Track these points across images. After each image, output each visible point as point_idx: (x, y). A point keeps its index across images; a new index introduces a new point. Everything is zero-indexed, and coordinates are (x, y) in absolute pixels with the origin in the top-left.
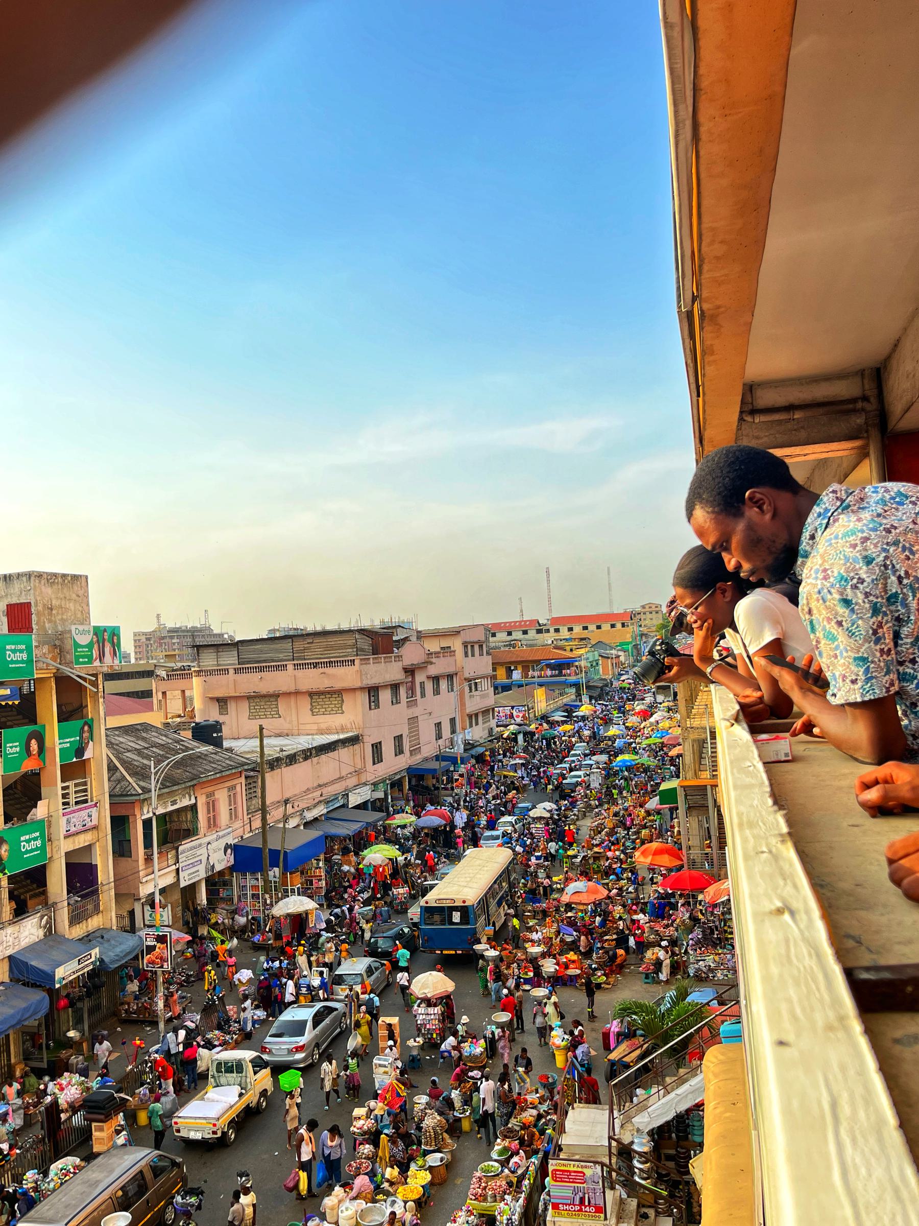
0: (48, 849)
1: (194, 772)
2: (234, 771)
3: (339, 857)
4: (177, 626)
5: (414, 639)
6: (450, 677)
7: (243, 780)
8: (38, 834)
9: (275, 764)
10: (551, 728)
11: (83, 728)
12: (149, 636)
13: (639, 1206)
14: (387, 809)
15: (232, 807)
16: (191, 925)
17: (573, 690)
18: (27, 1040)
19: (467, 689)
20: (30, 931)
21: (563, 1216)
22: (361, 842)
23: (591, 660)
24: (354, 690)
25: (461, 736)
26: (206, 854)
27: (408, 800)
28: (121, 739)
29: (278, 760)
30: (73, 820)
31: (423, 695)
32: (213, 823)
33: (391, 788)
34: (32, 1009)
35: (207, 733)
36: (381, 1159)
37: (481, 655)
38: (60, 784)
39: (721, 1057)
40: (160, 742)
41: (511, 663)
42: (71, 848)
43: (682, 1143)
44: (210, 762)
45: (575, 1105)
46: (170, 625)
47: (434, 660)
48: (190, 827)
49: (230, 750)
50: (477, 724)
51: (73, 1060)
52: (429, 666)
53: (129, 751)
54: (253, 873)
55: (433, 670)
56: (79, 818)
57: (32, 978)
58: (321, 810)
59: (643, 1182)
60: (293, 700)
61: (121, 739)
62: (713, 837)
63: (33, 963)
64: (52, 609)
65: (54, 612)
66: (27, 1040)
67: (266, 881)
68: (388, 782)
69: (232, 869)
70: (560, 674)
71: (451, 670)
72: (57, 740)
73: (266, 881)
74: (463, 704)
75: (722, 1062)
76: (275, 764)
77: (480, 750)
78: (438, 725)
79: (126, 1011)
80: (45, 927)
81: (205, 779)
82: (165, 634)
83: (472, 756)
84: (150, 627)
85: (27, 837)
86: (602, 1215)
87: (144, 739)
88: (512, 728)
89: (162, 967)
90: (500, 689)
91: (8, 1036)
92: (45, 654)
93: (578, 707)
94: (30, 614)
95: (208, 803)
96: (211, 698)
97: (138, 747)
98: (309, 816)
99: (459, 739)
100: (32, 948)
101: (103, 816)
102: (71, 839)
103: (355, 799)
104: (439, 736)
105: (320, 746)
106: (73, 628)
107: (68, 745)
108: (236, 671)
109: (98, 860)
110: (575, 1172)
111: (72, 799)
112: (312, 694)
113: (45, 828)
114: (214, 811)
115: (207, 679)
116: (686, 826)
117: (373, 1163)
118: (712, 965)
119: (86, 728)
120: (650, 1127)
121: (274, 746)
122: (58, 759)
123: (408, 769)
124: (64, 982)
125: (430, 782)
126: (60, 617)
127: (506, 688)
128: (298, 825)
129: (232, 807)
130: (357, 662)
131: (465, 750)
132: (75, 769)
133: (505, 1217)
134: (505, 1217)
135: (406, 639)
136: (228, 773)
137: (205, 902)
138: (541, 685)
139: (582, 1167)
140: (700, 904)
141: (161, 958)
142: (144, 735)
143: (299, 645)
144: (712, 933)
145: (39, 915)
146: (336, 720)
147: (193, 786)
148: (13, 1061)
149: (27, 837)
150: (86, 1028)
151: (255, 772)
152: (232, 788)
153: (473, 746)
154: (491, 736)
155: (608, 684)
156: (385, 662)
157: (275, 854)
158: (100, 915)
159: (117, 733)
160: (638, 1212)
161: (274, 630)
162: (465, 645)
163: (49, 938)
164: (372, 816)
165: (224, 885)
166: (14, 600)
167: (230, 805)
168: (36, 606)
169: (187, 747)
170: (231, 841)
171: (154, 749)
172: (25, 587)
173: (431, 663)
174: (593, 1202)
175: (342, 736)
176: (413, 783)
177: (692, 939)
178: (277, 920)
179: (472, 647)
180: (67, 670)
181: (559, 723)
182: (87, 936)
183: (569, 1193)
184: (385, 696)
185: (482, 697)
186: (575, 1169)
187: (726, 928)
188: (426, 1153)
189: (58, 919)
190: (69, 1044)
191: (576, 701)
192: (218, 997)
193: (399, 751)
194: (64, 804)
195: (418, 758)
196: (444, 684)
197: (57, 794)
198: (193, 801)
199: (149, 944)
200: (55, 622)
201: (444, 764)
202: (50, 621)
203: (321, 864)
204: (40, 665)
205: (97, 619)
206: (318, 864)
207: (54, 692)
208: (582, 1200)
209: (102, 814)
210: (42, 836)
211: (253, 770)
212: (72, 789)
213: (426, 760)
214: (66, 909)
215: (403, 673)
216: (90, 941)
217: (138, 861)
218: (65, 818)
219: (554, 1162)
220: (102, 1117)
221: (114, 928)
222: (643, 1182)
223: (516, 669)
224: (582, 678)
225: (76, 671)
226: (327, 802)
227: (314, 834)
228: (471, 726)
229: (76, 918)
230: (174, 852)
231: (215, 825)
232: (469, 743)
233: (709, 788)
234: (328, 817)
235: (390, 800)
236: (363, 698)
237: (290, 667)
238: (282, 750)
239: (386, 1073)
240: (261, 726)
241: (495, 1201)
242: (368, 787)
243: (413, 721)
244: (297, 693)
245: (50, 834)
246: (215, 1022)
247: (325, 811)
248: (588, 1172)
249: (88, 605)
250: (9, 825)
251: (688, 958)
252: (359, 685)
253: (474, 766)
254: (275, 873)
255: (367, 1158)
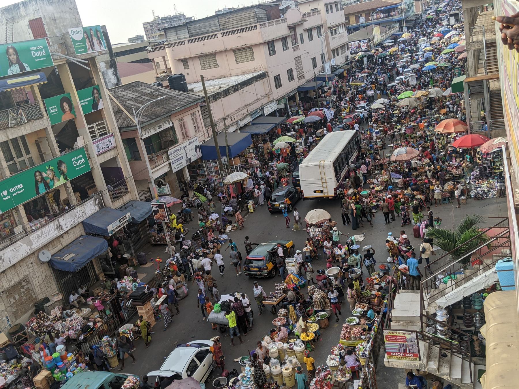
0: (90, 163)
1: (169, 108)
2: (192, 104)
3: (262, 145)
4: (166, 16)
5: (293, 6)
6: (318, 28)
7: (199, 108)
8: (81, 156)
9: (216, 97)
10: (384, 50)
11: (93, 91)
12: (151, 24)
13: (440, 350)
14: (288, 113)
15: (196, 125)
16: (185, 190)
17: (397, 25)
18: (103, 262)
19: (330, 34)
20: (90, 208)
21: (393, 358)
22: (272, 135)
23: (408, 3)
24: (259, 45)
25: (329, 64)
26: (184, 153)
27: (300, 107)
28: (124, 93)
29: (218, 94)
30: (100, 146)
31: (302, 42)
32: (186, 135)
33: (289, 101)
34: (99, 249)
35: (177, 83)
36: (291, 316)
37: (337, 10)
38: (87, 127)
39: (498, 303)
40: (147, 92)
41: (358, 12)
42: (103, 160)
43: (467, 310)
44: (177, 101)
45: (400, 291)
46: (162, 16)
47: (307, 19)
48: (173, 139)
49: (192, 90)
50: (338, 55)
51: (128, 270)
52: (304, 23)
53: (129, 100)
54: (213, 160)
55: (307, 25)
56: (104, 143)
57: (97, 232)
58: (249, 119)
59: (443, 337)
60: (224, 55)
61: (124, 93)
62: (487, 110)
63: (95, 225)
64: (55, 20)
65: (57, 21)
66: (103, 262)
67: (221, 164)
68: (286, 98)
69: (201, 159)
70: (388, 16)
71: (319, 23)
72: (79, 103)
73: (221, 164)
74: (328, 44)
75: (499, 307)
76: (216, 97)
77: (341, 71)
78: (314, 59)
79: (154, 240)
80: (98, 204)
81: (175, 112)
82: (160, 22)
83: (336, 75)
84: (151, 19)
85: (76, 158)
86: (418, 358)
87: (137, 91)
88: (360, 54)
89: (164, 220)
90: (350, 31)
91: (91, 262)
92: (56, 50)
93: (401, 35)
94: (43, 25)
95: (181, 125)
96: (178, 60)
97: (134, 97)
98: (242, 124)
99: (327, 66)
100: (93, 216)
101: (117, 140)
102: (102, 156)
103: (268, 111)
104: (315, 66)
105: (242, 82)
106: (70, 30)
107: (87, 103)
108: (189, 41)
109: (121, 165)
110: (400, 336)
111: (97, 133)
112: (235, 51)
113: (85, 151)
114: (185, 128)
115: (174, 48)
116: (471, 106)
117: (287, 318)
118: (485, 190)
119: (95, 91)
120: (447, 305)
121: (212, 87)
122: (82, 112)
123: (298, 88)
124: (114, 233)
125: (313, 95)
126: (62, 24)
127: (356, 29)
128: (236, 130)
129: (184, 131)
130: (258, 27)
131: (332, 72)
132: (94, 116)
133: (361, 352)
134: (361, 352)
135: (288, 7)
136: (188, 106)
137: (189, 178)
138: (377, 24)
139: (404, 334)
140: (478, 154)
141: (163, 216)
142: (137, 89)
143: (223, 20)
144: (486, 170)
145: (93, 199)
146: (249, 65)
147: (170, 116)
148: (97, 272)
149: (76, 158)
150: (133, 252)
151: (205, 103)
152: (193, 114)
153: (336, 69)
154: (348, 61)
155: (420, 17)
156: (276, 24)
157: (223, 148)
158: (129, 194)
159: (121, 89)
160: (440, 352)
161: (219, 11)
162: (326, 5)
163: (102, 210)
164: (278, 119)
165: (199, 168)
166: (32, 17)
167: (194, 124)
168: (45, 19)
169: (163, 93)
170: (198, 144)
171: (144, 97)
172: (35, 8)
173: (305, 21)
174: (412, 351)
175: (255, 74)
176: (302, 96)
177: (473, 175)
178: (227, 186)
179: (331, 6)
180: (72, 59)
181: (389, 47)
182: (124, 206)
183: (397, 347)
184: (279, 46)
185: (340, 37)
186: (400, 335)
187: (494, 167)
188: (316, 312)
189: (105, 199)
190: (125, 261)
191: (399, 31)
192: (199, 231)
193: (291, 78)
194: (92, 137)
195: (303, 81)
196: (315, 33)
197: (86, 132)
198: (171, 125)
199: (155, 209)
200: (60, 28)
201: (318, 82)
202: (56, 28)
203: (251, 151)
204: (55, 57)
205: (87, 21)
206: (249, 151)
207: (69, 72)
208: (405, 351)
209: (117, 140)
210: (84, 156)
211: (204, 102)
212: (96, 128)
213: (308, 81)
214: (108, 194)
215: (288, 30)
216: (126, 208)
217: (145, 162)
218: (95, 145)
219: (387, 331)
220: (141, 303)
221: (139, 199)
222: (443, 337)
223: (361, 16)
224: (403, 16)
225: (79, 58)
226: (251, 115)
227: (245, 135)
228: (334, 57)
229: (115, 197)
230: (165, 154)
231: (187, 136)
232: (334, 68)
233: (485, 81)
234: (254, 123)
235: (289, 108)
236: (265, 49)
237: (219, 35)
238: (220, 88)
239: (293, 266)
240: (201, 76)
241: (356, 339)
242: (275, 103)
243: (298, 59)
244: (226, 51)
245: (89, 155)
246: (200, 243)
247: (251, 120)
248: (408, 336)
249: (78, 14)
250: (64, 153)
251: (471, 186)
252: (261, 41)
253: (337, 81)
254: (224, 160)
255: (284, 316)
